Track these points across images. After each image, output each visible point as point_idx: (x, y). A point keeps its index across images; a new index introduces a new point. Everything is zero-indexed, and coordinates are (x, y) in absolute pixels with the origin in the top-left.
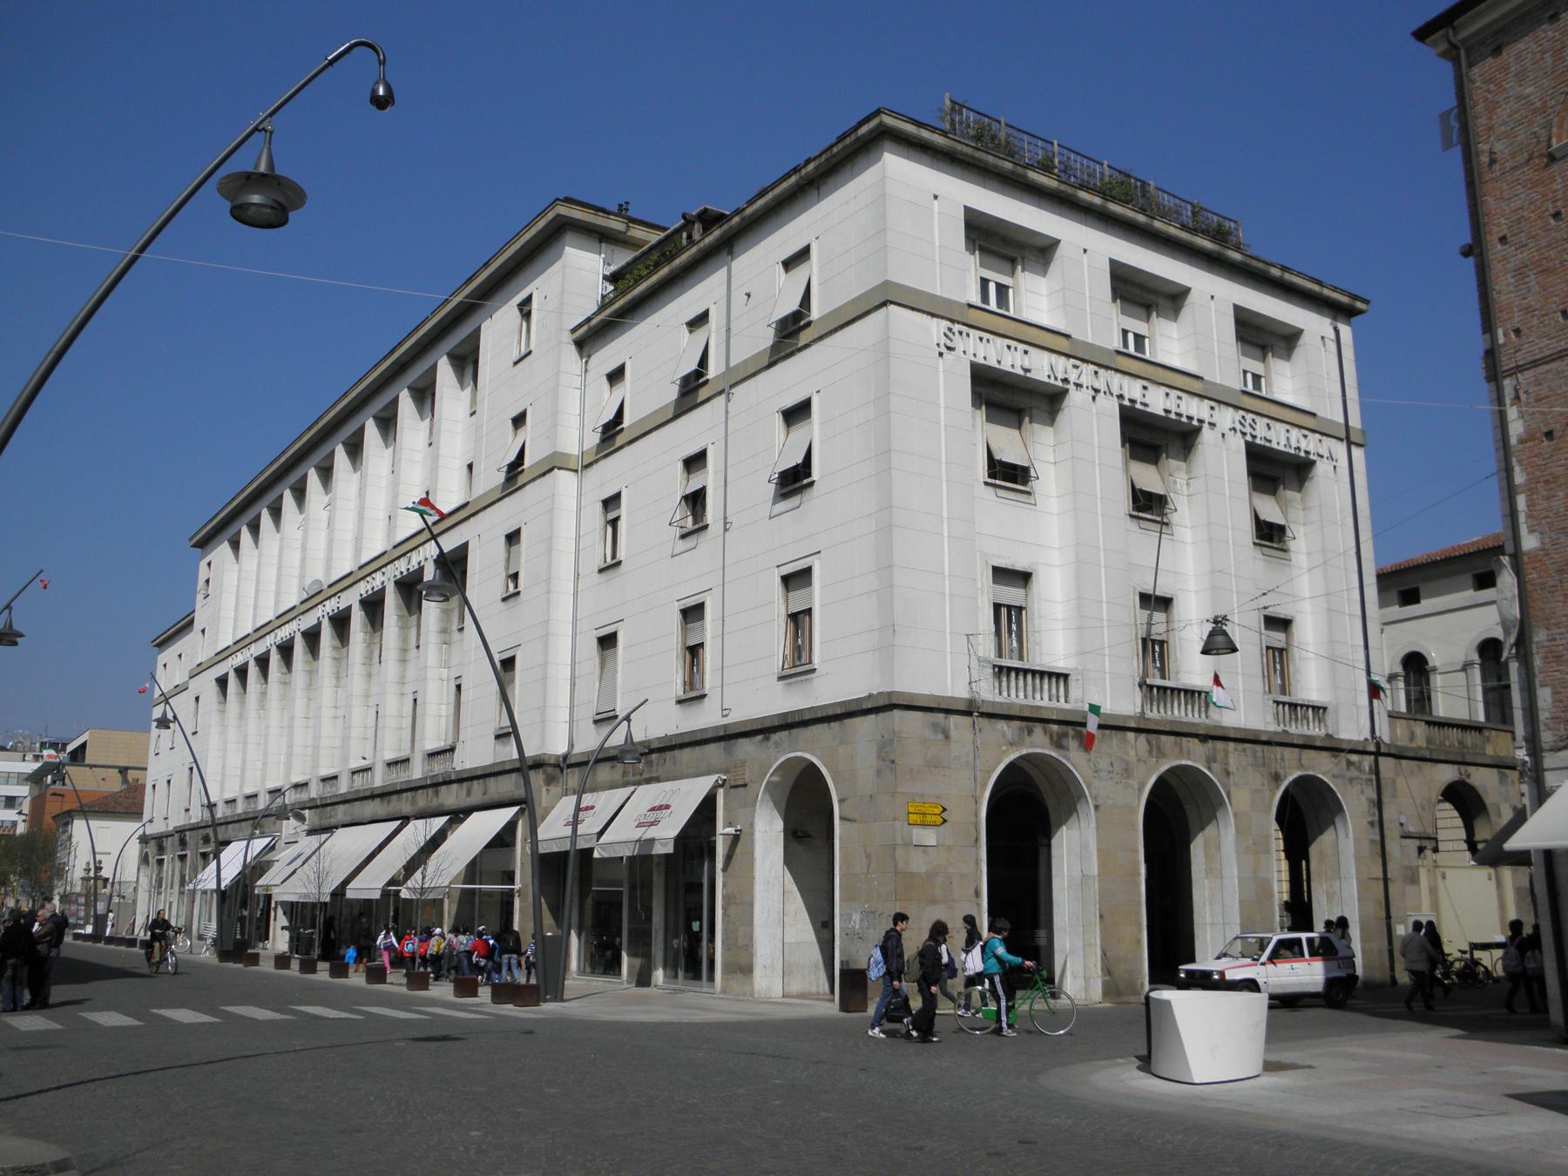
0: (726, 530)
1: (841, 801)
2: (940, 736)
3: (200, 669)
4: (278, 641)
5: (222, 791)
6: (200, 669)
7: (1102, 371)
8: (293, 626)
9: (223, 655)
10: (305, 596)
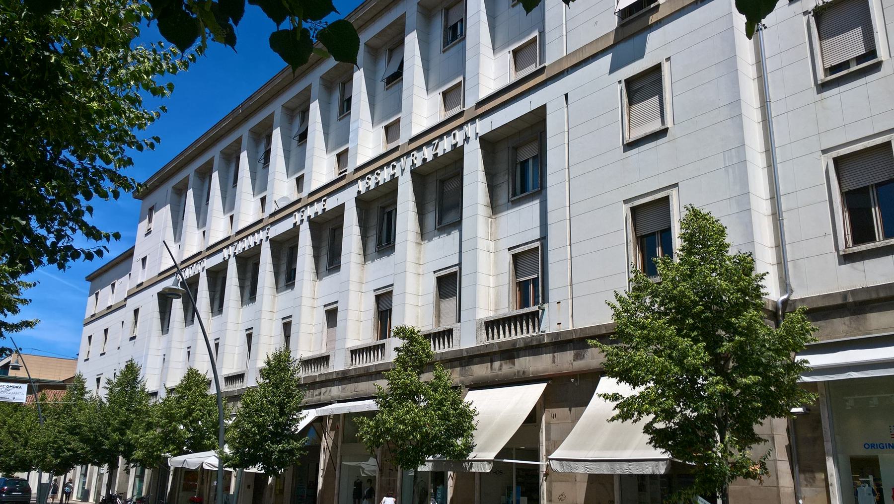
3: (141, 288)
6: (141, 288)
8: (262, 235)
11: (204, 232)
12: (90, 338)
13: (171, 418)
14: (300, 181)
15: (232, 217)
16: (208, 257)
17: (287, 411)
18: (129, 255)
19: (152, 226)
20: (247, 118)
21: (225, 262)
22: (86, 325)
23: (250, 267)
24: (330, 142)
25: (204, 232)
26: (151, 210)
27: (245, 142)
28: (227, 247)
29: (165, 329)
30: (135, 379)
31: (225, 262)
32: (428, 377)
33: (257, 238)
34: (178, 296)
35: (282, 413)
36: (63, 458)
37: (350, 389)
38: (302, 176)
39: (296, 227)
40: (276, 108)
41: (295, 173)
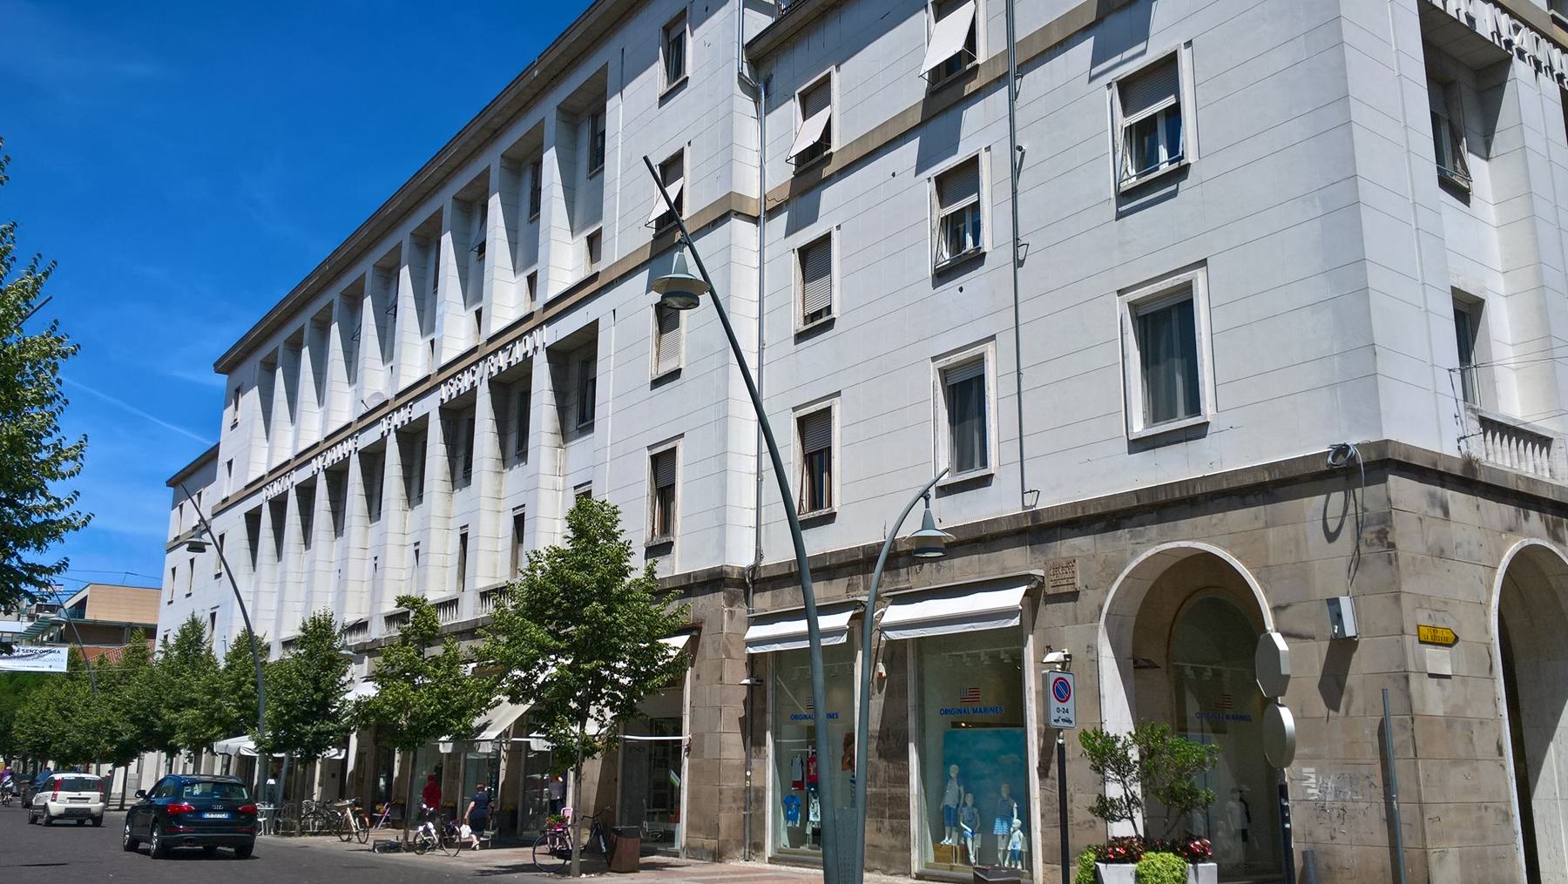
0: (1019, 263)
1: (1276, 609)
2: (1439, 513)
3: (227, 505)
4: (328, 463)
5: (278, 631)
6: (227, 505)
7: (1543, 42)
8: (349, 446)
9: (254, 487)
10: (364, 410)
11: (432, 342)
12: (174, 570)
13: (216, 693)
14: (594, 242)
15: (479, 313)
16: (549, 322)
17: (322, 685)
18: (213, 454)
19: (239, 415)
20: (496, 134)
21: (314, 478)
22: (169, 551)
23: (575, 370)
24: (520, 254)
25: (432, 342)
26: (238, 392)
27: (495, 178)
28: (315, 457)
29: (375, 512)
30: (199, 639)
31: (314, 478)
32: (438, 651)
33: (465, 381)
34: (277, 514)
35: (317, 689)
36: (122, 744)
37: (963, 568)
38: (599, 233)
39: (384, 438)
40: (547, 112)
41: (584, 228)
